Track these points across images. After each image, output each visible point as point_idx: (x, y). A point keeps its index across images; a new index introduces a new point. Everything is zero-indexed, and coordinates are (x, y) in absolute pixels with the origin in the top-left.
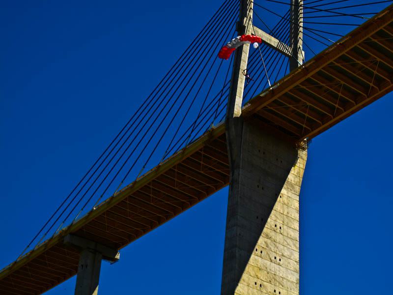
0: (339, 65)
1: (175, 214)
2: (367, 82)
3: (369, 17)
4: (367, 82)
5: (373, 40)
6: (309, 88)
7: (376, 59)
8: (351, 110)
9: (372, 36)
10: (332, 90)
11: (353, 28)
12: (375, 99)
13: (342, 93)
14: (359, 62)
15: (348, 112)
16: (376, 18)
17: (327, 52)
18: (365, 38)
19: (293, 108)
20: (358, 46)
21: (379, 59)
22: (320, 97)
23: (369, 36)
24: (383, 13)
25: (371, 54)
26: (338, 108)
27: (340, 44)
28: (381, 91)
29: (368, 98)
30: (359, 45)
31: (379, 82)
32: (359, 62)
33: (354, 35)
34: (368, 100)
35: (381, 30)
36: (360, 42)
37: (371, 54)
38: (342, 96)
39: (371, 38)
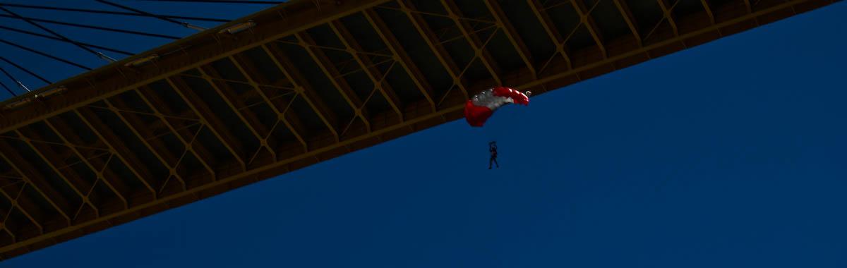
0: (116, 110)
1: (760, 25)
2: (78, 192)
3: (113, 59)
4: (78, 192)
5: (302, 43)
6: (313, 50)
7: (108, 148)
8: (59, 233)
9: (111, 100)
10: (269, 102)
11: (78, 72)
12: (262, 177)
13: (105, 175)
14: (255, 85)
15: (22, 244)
16: (127, 65)
17: (9, 106)
18: (287, 34)
19: (165, 121)
20: (170, 82)
21: (113, 151)
22: (56, 170)
23: (105, 97)
24: (145, 57)
25: (14, 166)
26: (173, 177)
27: (132, 66)
28: (161, 201)
29: (72, 225)
30: (80, 110)
31: (377, 111)
32: (255, 85)
33: (74, 88)
34: (70, 229)
35: (164, 80)
36: (82, 104)
37: (14, 166)
38: (285, 121)
39: (19, 133)
